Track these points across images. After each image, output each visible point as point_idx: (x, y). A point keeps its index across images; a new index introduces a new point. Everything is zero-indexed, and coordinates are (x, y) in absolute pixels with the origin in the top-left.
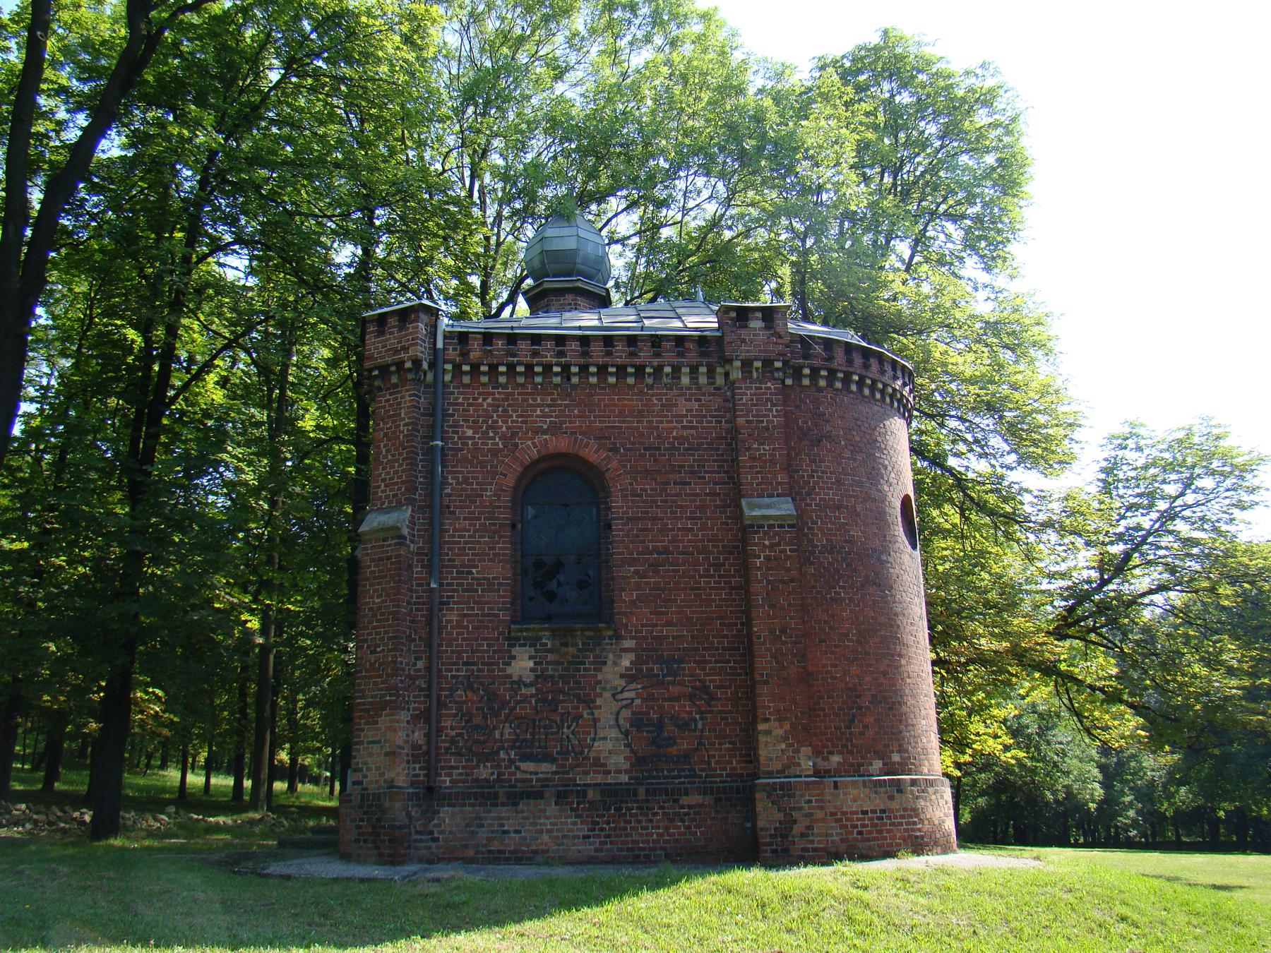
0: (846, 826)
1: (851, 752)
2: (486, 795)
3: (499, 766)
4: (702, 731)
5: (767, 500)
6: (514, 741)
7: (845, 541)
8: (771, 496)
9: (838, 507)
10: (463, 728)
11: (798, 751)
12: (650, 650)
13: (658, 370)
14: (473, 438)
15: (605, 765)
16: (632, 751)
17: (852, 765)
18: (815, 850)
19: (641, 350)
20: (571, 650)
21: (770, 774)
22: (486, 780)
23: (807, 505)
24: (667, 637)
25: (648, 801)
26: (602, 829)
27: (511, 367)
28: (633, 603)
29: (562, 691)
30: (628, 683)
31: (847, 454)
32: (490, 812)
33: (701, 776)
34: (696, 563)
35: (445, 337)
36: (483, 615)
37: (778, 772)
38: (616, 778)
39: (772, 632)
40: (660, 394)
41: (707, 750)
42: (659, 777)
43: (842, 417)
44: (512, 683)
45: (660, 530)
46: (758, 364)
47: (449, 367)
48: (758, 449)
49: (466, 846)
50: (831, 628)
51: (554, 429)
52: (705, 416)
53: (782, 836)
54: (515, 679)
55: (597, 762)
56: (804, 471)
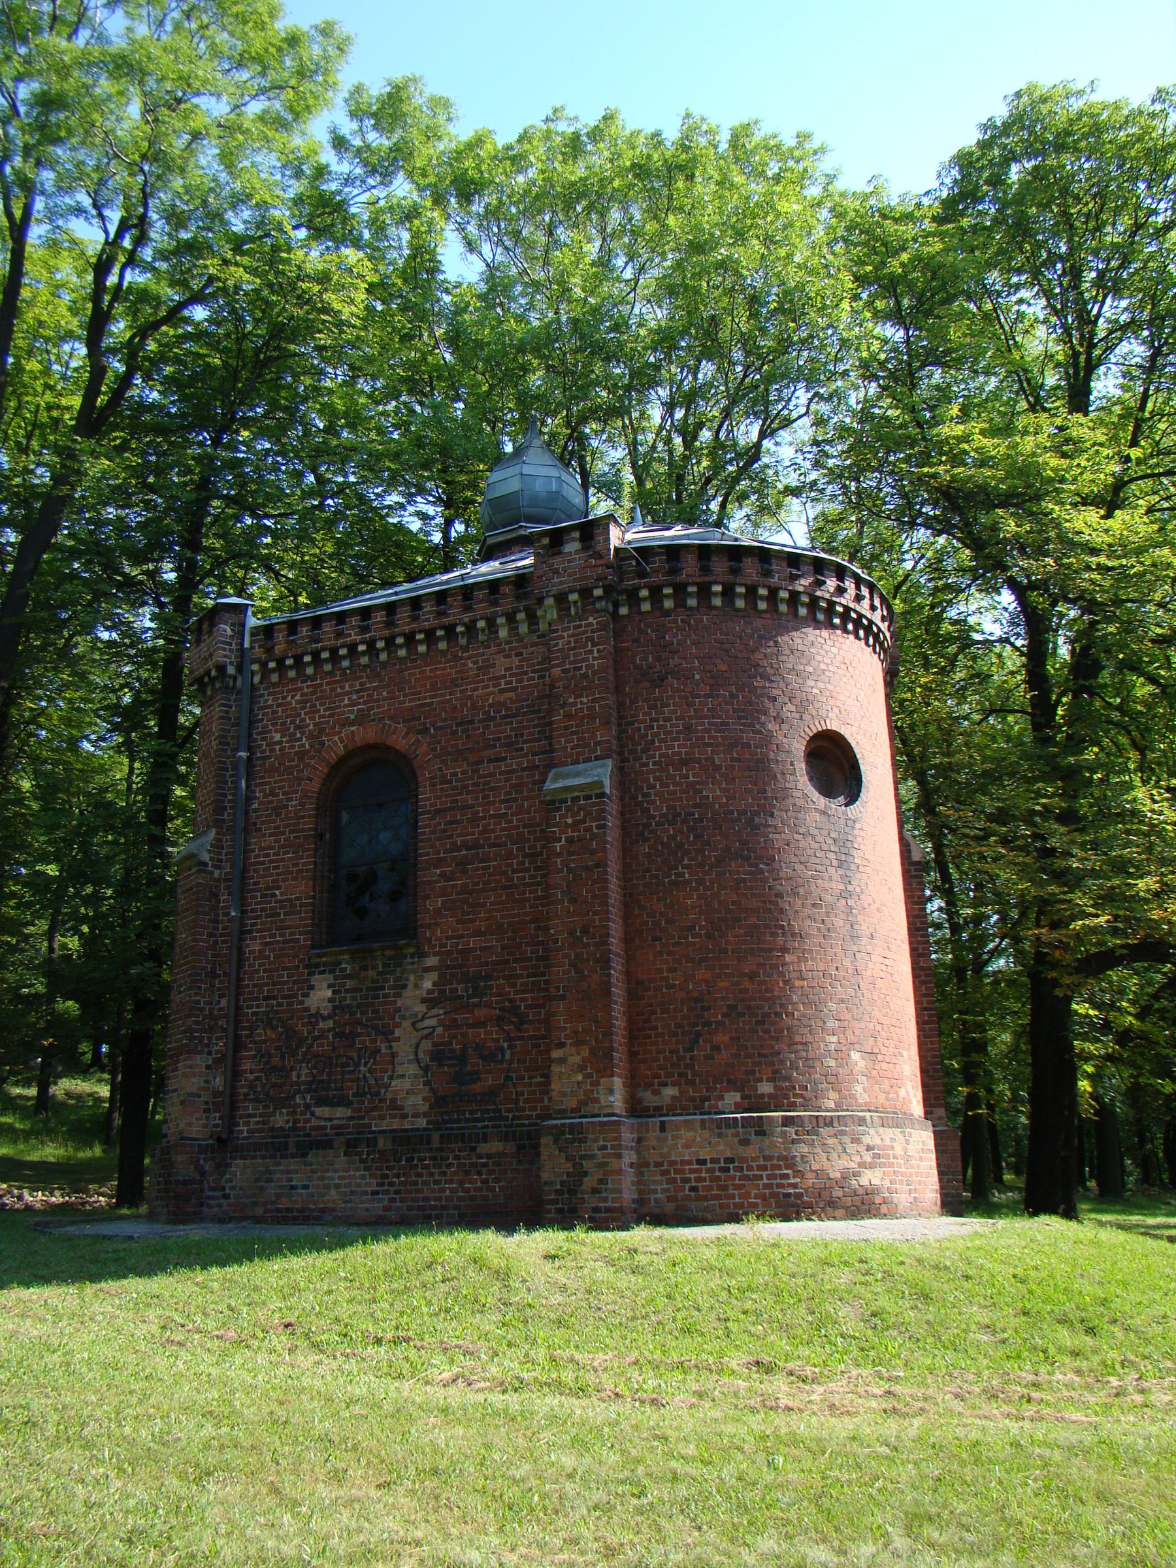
0: (674, 1180)
1: (691, 1083)
2: (278, 1146)
3: (295, 1113)
4: (511, 1062)
5: (581, 766)
6: (310, 1083)
7: (696, 806)
8: (589, 760)
9: (684, 763)
10: (261, 1071)
11: (597, 1083)
12: (454, 967)
13: (471, 628)
14: (280, 743)
15: (401, 1108)
16: (432, 1090)
17: (692, 1099)
18: (608, 1210)
19: (451, 607)
20: (371, 973)
21: (563, 1114)
22: (282, 1129)
23: (642, 765)
24: (474, 950)
25: (441, 1150)
26: (391, 1184)
27: (316, 655)
28: (437, 912)
29: (361, 1023)
30: (429, 1008)
31: (704, 690)
32: (279, 1164)
33: (506, 1119)
34: (510, 855)
35: (252, 635)
36: (285, 942)
37: (573, 1111)
38: (413, 1123)
39: (572, 933)
40: (477, 655)
41: (514, 1086)
42: (458, 1121)
43: (696, 643)
44: (311, 1016)
45: (469, 821)
46: (574, 597)
47: (255, 667)
48: (575, 704)
49: (255, 1204)
50: (669, 922)
51: (362, 719)
52: (526, 673)
53: (570, 1192)
54: (313, 1011)
55: (394, 1105)
56: (640, 722)
